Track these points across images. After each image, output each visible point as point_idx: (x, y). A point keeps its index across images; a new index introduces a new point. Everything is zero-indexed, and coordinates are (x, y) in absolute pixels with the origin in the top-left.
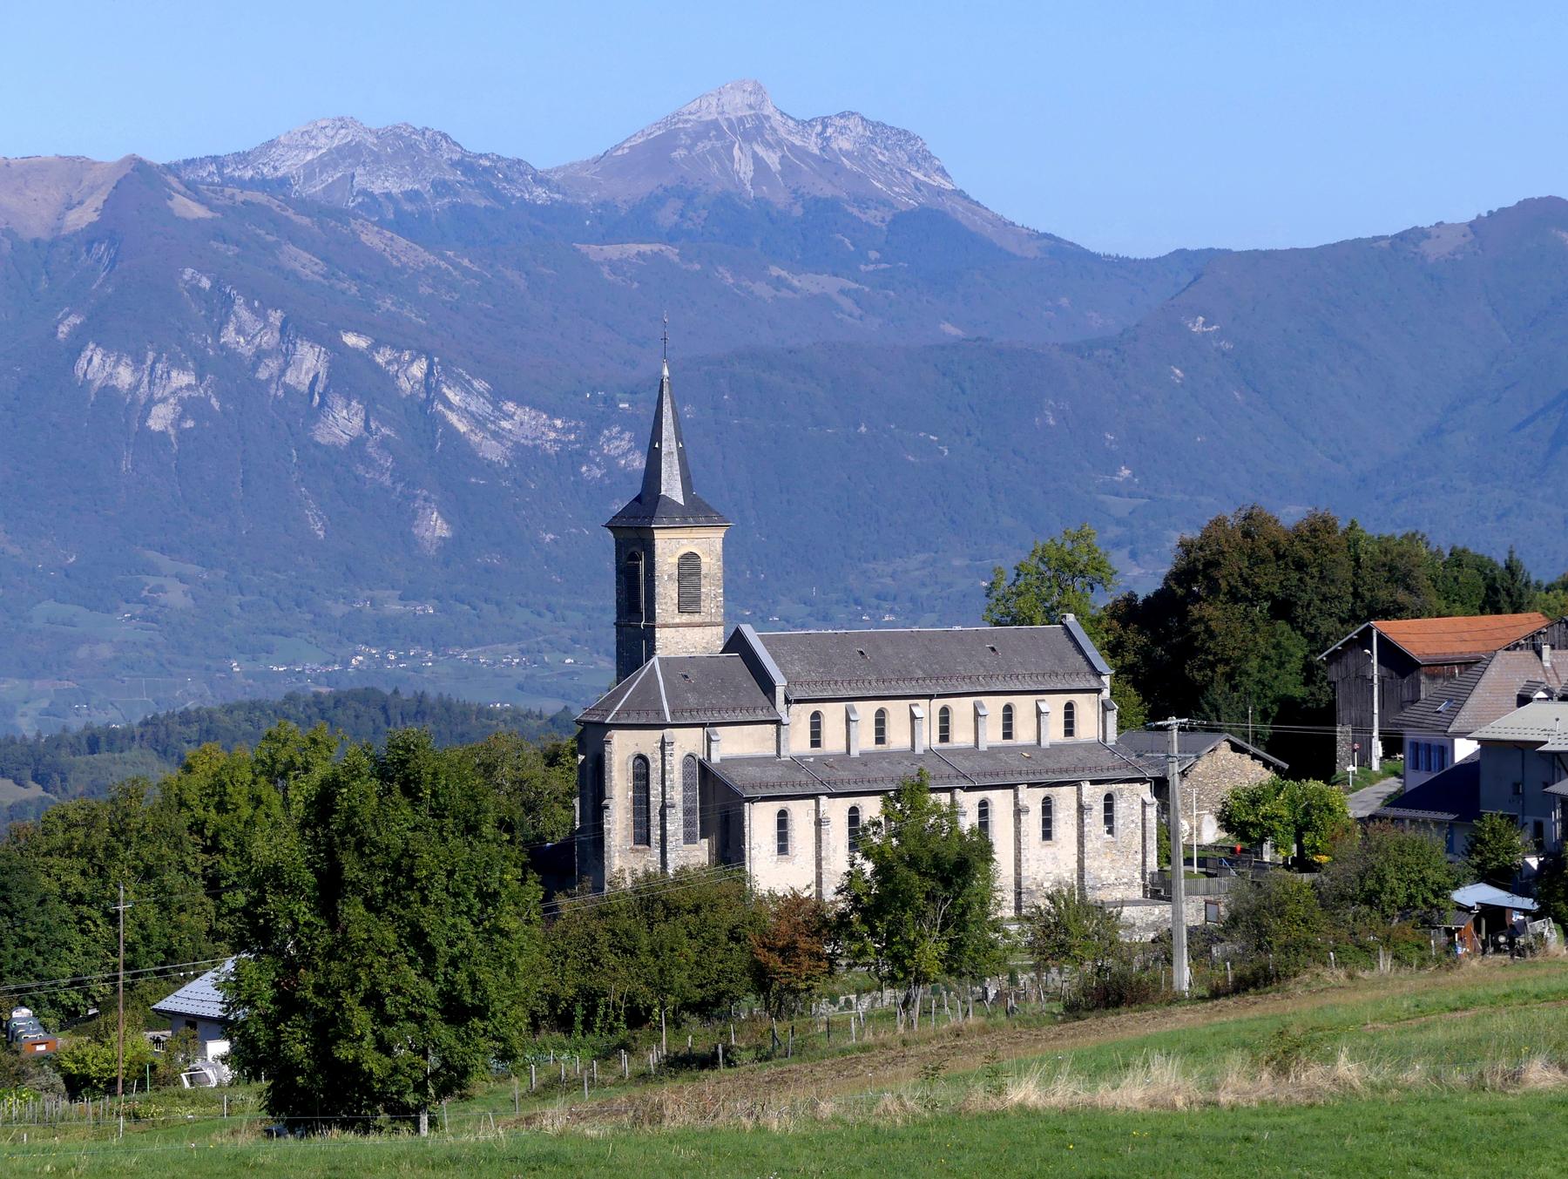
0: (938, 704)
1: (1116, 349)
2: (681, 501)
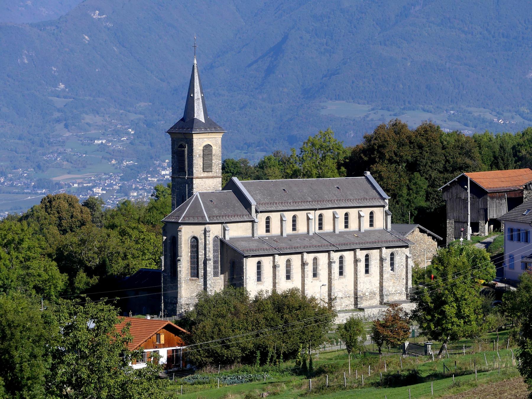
0: (318, 212)
1: (57, 26)
2: (203, 121)
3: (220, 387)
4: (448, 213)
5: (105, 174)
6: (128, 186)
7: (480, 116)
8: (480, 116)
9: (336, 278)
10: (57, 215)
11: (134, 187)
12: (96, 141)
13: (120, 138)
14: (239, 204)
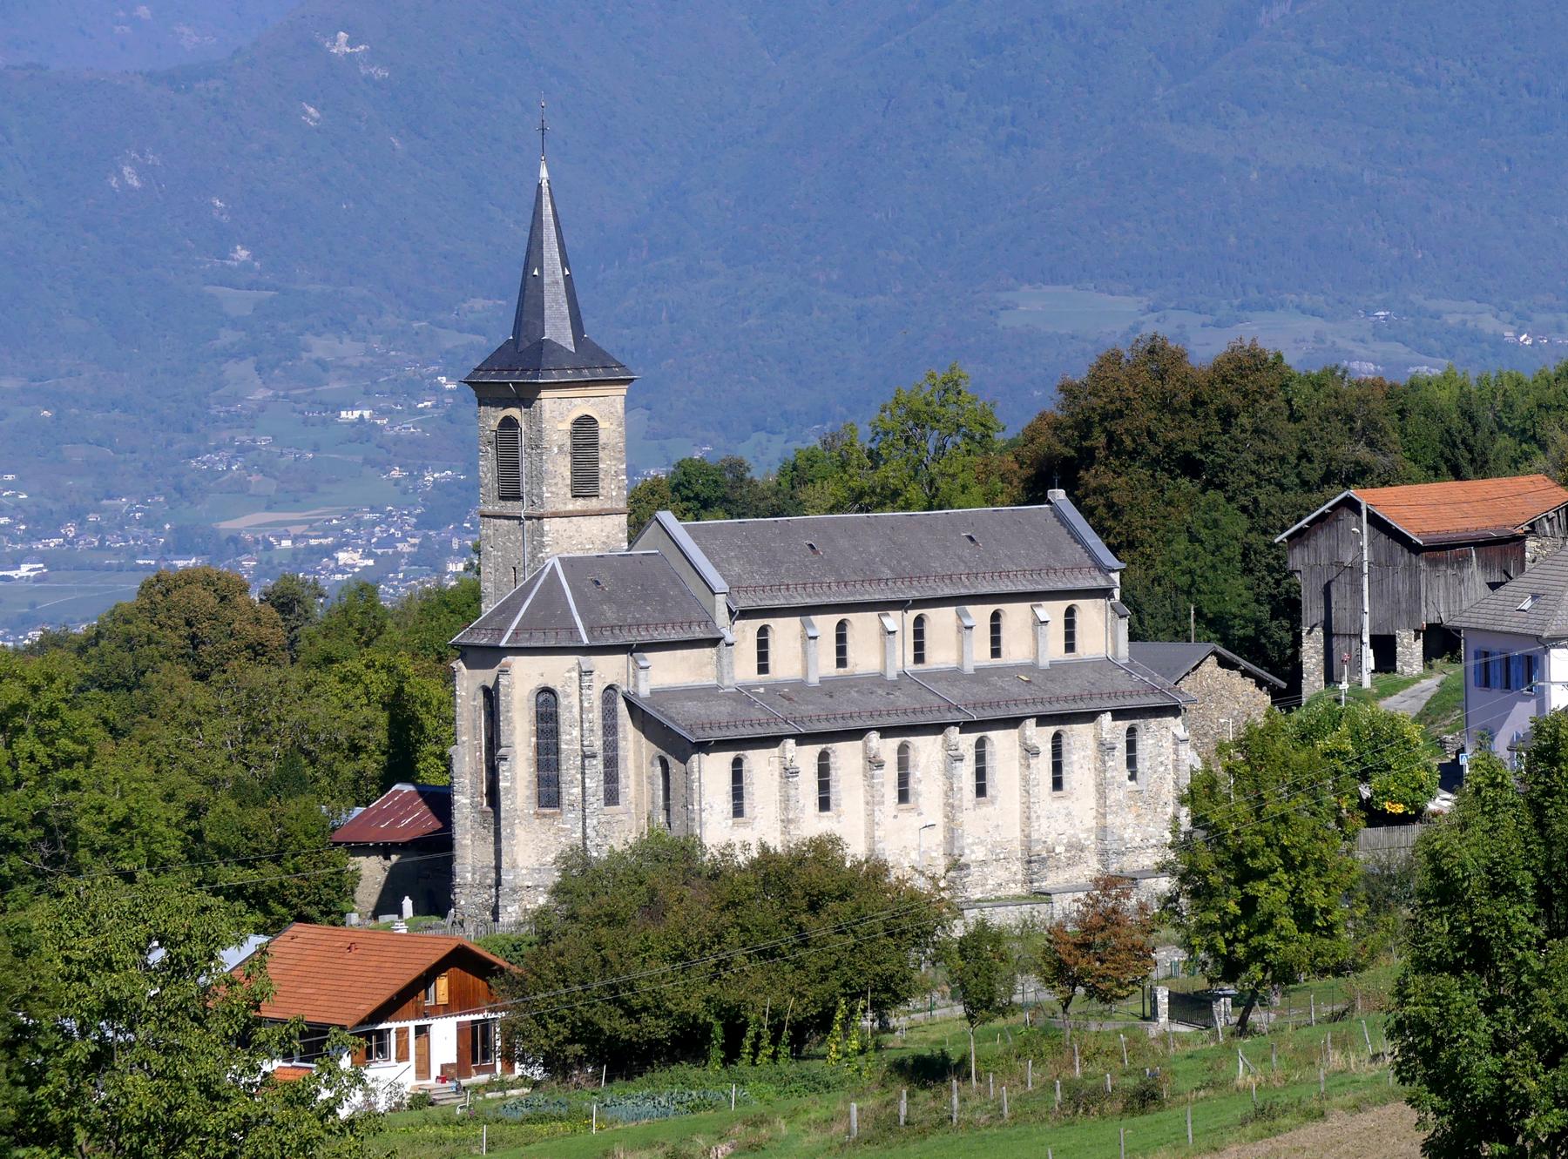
0: (913, 614)
3: (601, 1129)
5: (373, 510)
6: (440, 544)
7: (1464, 323)
8: (1464, 323)
9: (966, 804)
10: (185, 631)
11: (455, 546)
12: (343, 414)
13: (414, 403)
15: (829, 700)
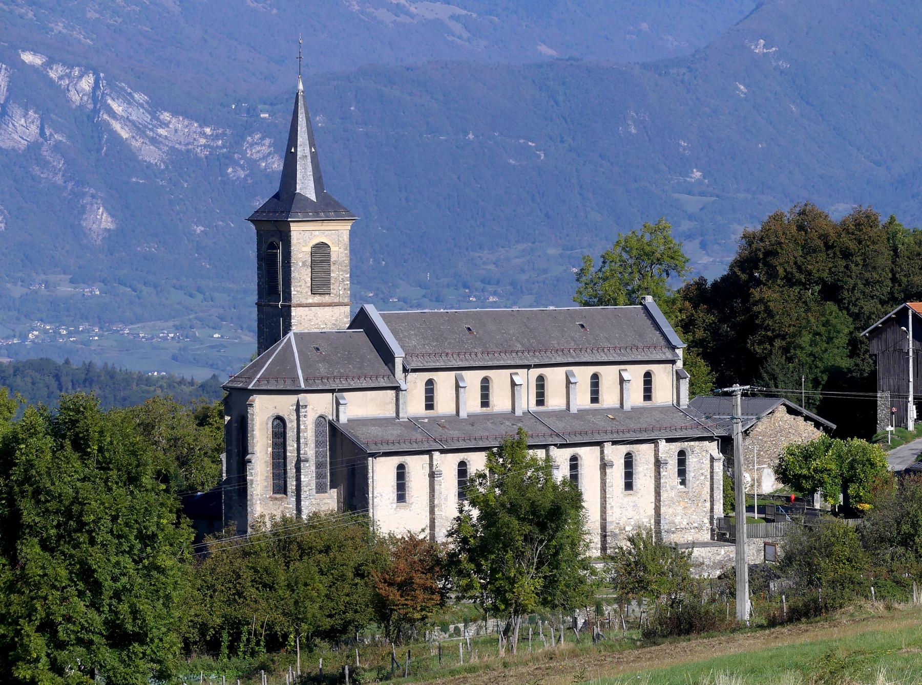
0: (535, 373)
1: (689, 67)
4: (879, 379)
14: (373, 355)
15: (471, 428)
